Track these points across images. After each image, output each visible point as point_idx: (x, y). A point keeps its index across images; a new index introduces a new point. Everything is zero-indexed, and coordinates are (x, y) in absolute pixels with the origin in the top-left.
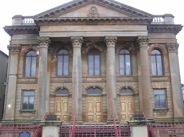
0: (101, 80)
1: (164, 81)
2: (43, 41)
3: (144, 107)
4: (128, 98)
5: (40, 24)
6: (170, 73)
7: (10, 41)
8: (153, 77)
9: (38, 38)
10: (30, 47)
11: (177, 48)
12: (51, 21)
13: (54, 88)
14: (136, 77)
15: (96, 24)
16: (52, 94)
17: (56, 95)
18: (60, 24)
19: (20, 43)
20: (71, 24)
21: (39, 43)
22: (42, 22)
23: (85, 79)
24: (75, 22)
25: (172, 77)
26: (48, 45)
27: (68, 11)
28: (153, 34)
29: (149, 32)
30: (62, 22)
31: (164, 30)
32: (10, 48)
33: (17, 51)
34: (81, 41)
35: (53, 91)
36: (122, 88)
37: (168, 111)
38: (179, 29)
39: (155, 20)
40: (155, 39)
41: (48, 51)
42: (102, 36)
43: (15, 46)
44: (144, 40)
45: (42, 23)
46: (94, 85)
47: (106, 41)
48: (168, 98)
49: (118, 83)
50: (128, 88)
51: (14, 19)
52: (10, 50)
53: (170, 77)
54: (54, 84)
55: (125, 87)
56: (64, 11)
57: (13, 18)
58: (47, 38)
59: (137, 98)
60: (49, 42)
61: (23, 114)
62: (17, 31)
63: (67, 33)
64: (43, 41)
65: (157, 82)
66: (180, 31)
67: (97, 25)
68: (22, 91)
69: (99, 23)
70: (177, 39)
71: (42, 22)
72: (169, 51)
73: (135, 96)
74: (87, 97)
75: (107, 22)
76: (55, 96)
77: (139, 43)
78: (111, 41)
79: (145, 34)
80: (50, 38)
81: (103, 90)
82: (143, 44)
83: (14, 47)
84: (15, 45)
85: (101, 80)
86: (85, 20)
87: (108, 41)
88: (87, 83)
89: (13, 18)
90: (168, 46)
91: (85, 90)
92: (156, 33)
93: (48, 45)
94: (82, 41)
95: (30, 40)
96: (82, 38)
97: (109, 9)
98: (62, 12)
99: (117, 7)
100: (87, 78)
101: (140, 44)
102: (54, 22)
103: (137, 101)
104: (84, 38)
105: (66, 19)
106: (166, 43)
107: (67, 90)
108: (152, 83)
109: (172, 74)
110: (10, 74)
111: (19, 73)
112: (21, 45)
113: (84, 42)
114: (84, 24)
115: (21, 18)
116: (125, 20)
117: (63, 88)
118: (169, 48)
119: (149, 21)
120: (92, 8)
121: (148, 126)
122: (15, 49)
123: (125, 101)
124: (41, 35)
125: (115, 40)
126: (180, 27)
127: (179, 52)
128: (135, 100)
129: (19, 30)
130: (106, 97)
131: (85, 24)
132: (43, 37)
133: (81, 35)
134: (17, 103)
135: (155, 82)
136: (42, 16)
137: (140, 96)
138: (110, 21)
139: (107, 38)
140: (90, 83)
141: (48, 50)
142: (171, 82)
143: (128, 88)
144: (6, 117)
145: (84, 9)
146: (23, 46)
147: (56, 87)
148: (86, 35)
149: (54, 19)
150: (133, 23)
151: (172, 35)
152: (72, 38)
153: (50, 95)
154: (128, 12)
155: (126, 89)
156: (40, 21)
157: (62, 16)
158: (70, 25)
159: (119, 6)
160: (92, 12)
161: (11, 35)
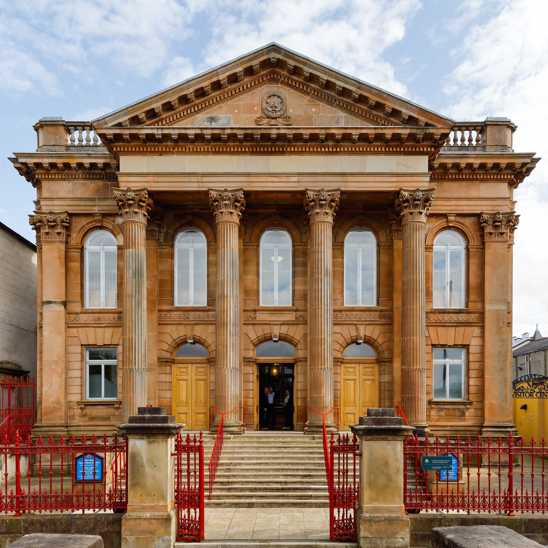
0: (294, 319)
1: (467, 324)
2: (132, 202)
3: (403, 392)
4: (197, 368)
5: (118, 149)
6: (483, 301)
7: (37, 203)
8: (431, 312)
9: (117, 193)
10: (95, 221)
11: (513, 229)
12: (150, 138)
13: (170, 341)
14: (387, 313)
15: (281, 150)
16: (165, 357)
17: (174, 360)
18: (176, 149)
19: (67, 209)
20: (210, 150)
21: (120, 209)
22: (124, 140)
23: (252, 314)
24: (351, 144)
25: (487, 315)
26: (145, 215)
27: (200, 108)
28: (447, 185)
29: (432, 180)
30: (180, 144)
31: (481, 172)
32: (38, 224)
33: (59, 234)
34: (239, 204)
35: (166, 347)
36: (349, 341)
37: (469, 408)
38: (524, 170)
39: (455, 140)
40: (448, 199)
41: (146, 234)
42: (298, 189)
43: (51, 217)
44: (416, 202)
45: (122, 144)
46: (276, 331)
47: (307, 205)
48: (471, 372)
49: (338, 329)
50: (364, 342)
51: (40, 131)
52: (37, 229)
53: (482, 313)
54: (169, 329)
55: (357, 339)
56: (187, 106)
57: (37, 128)
58: (143, 193)
59: (387, 367)
60: (149, 205)
61: (89, 411)
62: (52, 172)
63: (200, 179)
64: (132, 202)
65: (445, 328)
66: (528, 176)
67: (282, 153)
68: (84, 347)
69: (289, 150)
70: (514, 200)
71: (124, 140)
72: (487, 239)
73: (383, 364)
74: (343, 365)
75: (313, 144)
76: (173, 362)
77: (401, 210)
78: (321, 206)
79: (424, 183)
80: (151, 194)
81: (299, 346)
82: (411, 213)
83: (49, 221)
84: (51, 213)
85: (294, 319)
86: (249, 137)
87: (313, 206)
88: (256, 327)
89: (37, 128)
90: (486, 222)
91: (252, 347)
92: (456, 180)
93: (145, 215)
94: (242, 205)
95: (93, 199)
96: (241, 195)
97: (320, 99)
98: (181, 108)
99: (345, 92)
100: (258, 313)
101: (403, 216)
102: (160, 141)
103: (386, 378)
104: (247, 194)
105: (342, 131)
106: (482, 213)
107: (202, 344)
108: (431, 328)
109: (488, 307)
110: (45, 300)
111: (70, 299)
112: (71, 215)
113: (246, 207)
114: (247, 150)
115: (62, 129)
116: (364, 138)
117: (194, 339)
118: (489, 229)
119: (436, 141)
120: (269, 97)
121: (404, 441)
122: (52, 227)
123: (186, 377)
124: (124, 183)
125: (333, 201)
126: (528, 161)
127: (515, 240)
128: (383, 376)
129: (58, 167)
130: (307, 365)
131: (251, 150)
132: (129, 190)
133: (239, 185)
134: (70, 382)
135: (439, 328)
136: (120, 120)
137: (397, 364)
138: (323, 141)
139: (311, 194)
140: (264, 327)
141: (147, 231)
142: (483, 327)
143: (364, 342)
144: (44, 418)
145: (245, 99)
146: (75, 219)
147: (176, 336)
148: (252, 185)
149: (158, 133)
150: (323, 150)
151: (502, 189)
152: (214, 194)
153: (158, 359)
154: (374, 112)
155: (360, 344)
156: (118, 138)
157: (181, 124)
158: (207, 153)
159: (351, 91)
160: (270, 110)
161: (37, 184)
